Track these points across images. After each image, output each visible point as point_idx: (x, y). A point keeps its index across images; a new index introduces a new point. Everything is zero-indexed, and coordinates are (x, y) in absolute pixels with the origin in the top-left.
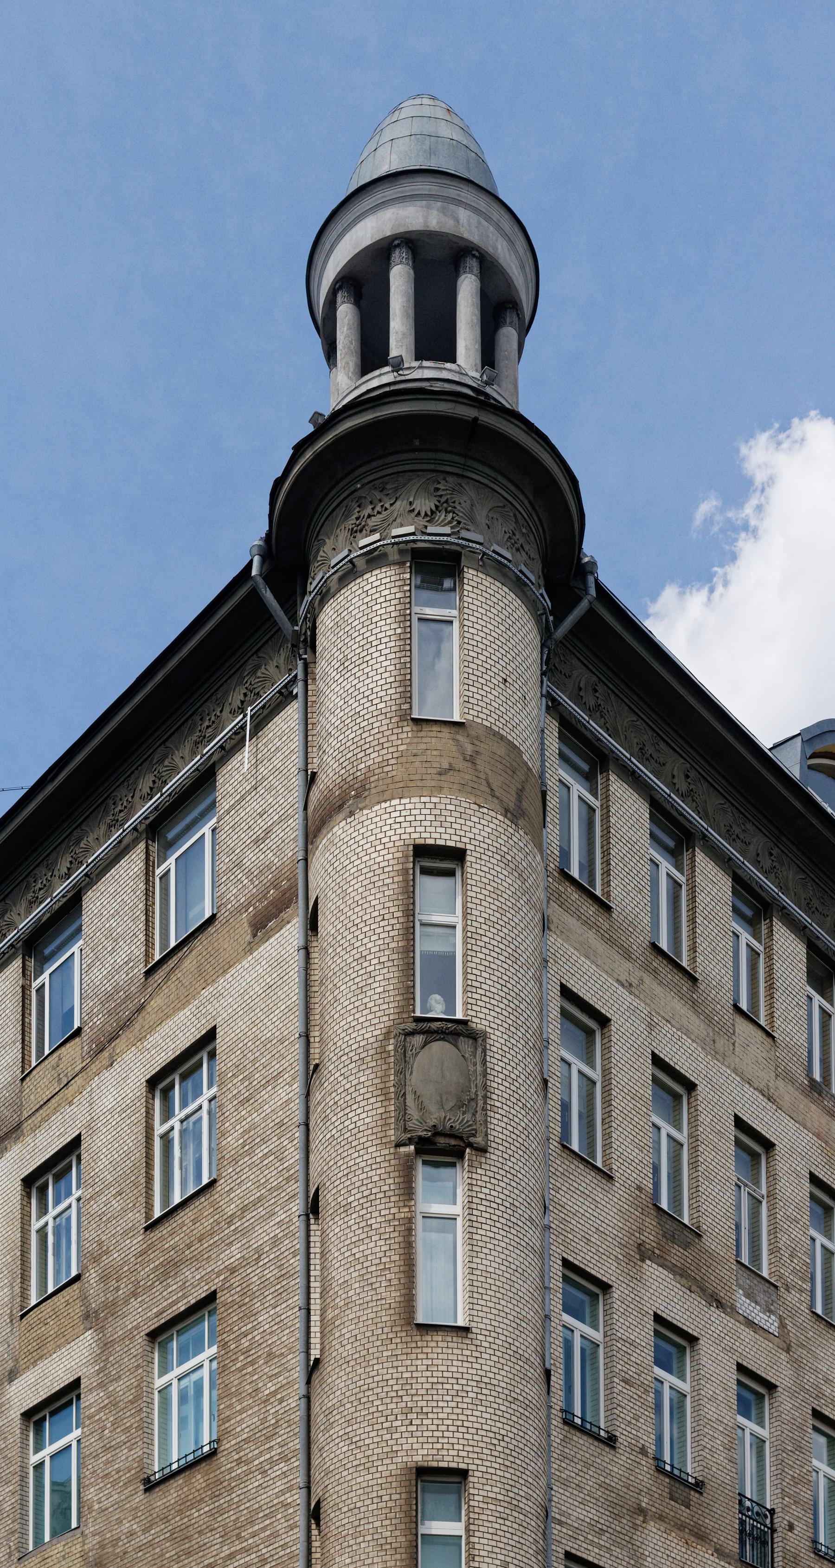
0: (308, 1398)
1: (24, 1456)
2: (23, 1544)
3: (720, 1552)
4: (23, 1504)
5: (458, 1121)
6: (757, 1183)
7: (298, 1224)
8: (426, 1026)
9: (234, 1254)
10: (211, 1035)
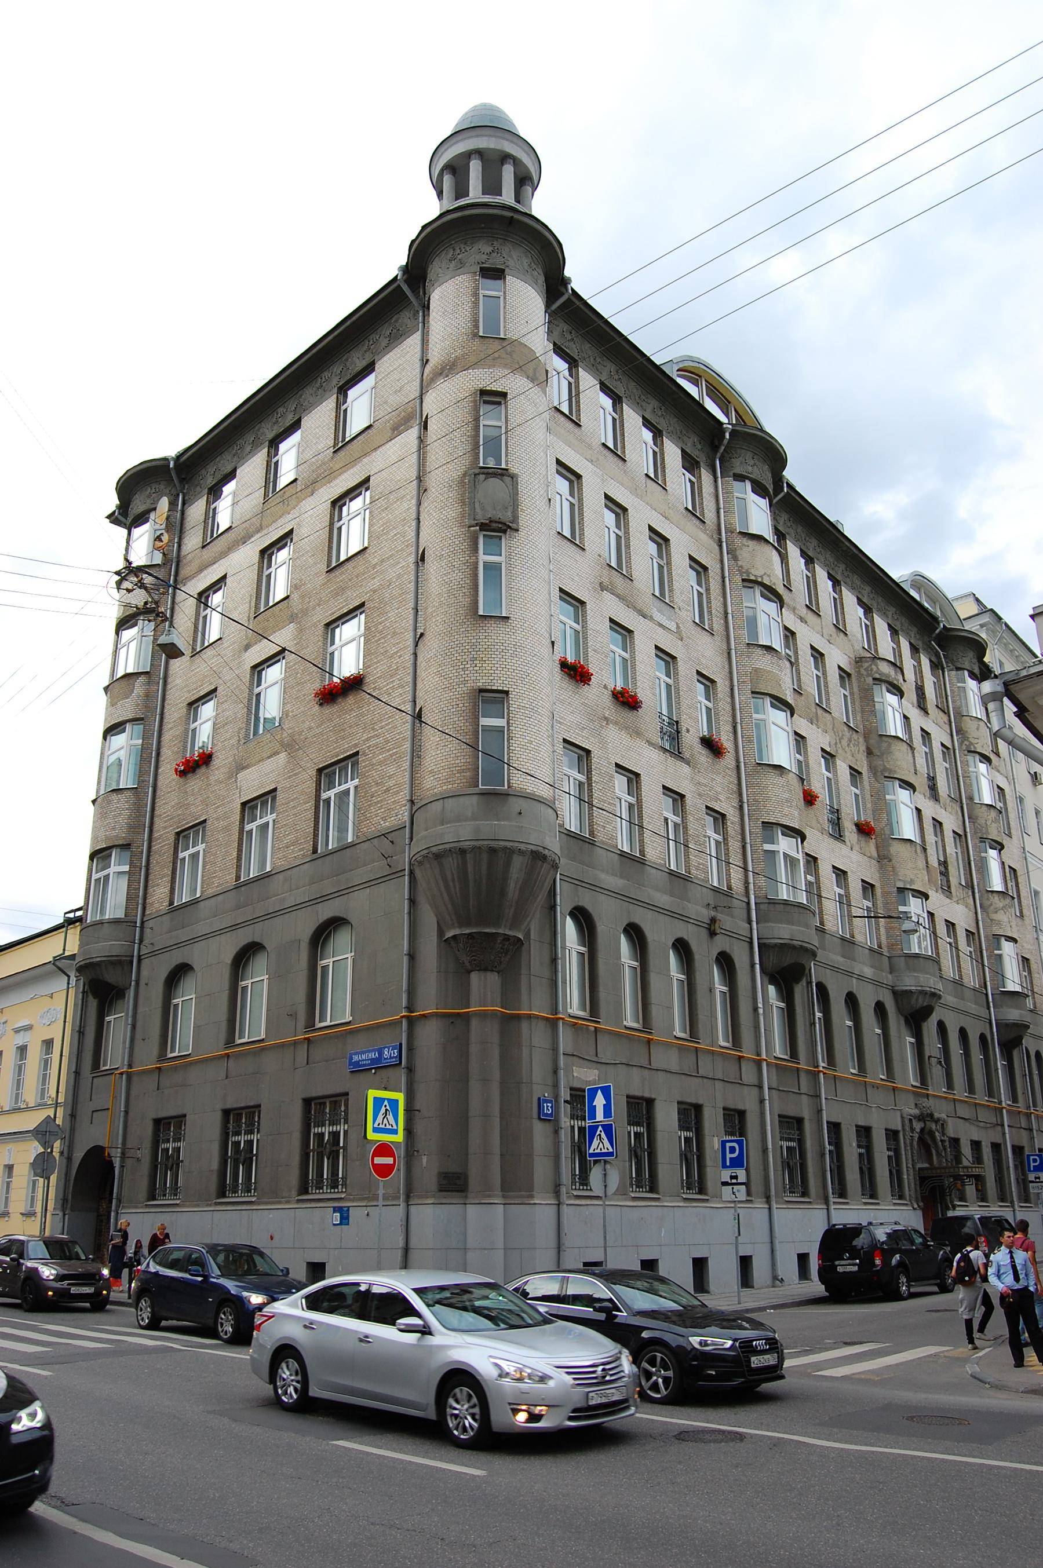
0: (415, 654)
2: (247, 735)
5: (506, 516)
7: (412, 567)
8: (486, 471)
9: (376, 583)
10: (367, 480)
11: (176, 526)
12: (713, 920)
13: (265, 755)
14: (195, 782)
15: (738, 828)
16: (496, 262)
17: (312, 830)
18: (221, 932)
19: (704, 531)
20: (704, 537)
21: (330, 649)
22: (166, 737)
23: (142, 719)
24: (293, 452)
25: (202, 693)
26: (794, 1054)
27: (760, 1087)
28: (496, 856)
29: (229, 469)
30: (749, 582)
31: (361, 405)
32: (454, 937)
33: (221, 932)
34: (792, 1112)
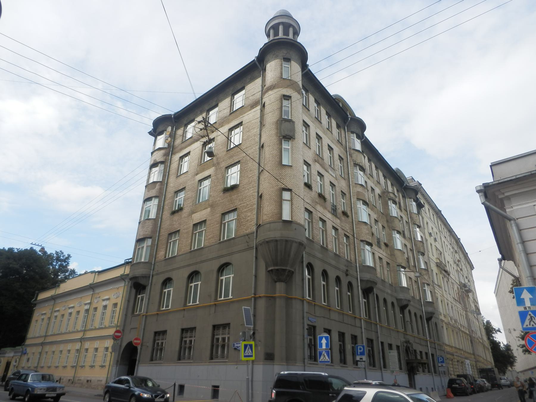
1: (198, 188)
2: (196, 202)
3: (329, 212)
4: (197, 196)
5: (291, 134)
11: (173, 136)
12: (347, 270)
14: (176, 217)
15: (353, 241)
16: (288, 56)
18: (184, 267)
20: (342, 149)
21: (227, 175)
22: (166, 203)
24: (241, 98)
26: (370, 317)
27: (361, 328)
28: (287, 242)
29: (192, 118)
30: (356, 165)
31: (239, 100)
32: (272, 270)
33: (184, 267)
34: (370, 337)
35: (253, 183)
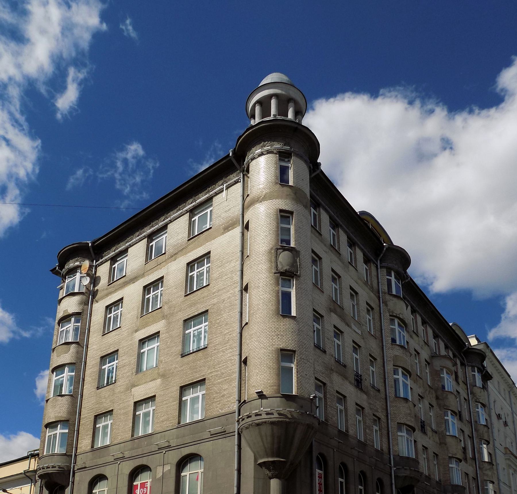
3: (350, 383)
6: (354, 301)
7: (239, 293)
9: (215, 301)
13: (148, 380)
15: (386, 425)
17: (177, 414)
19: (372, 292)
22: (88, 372)
23: (74, 363)
25: (109, 352)
35: (231, 342)
